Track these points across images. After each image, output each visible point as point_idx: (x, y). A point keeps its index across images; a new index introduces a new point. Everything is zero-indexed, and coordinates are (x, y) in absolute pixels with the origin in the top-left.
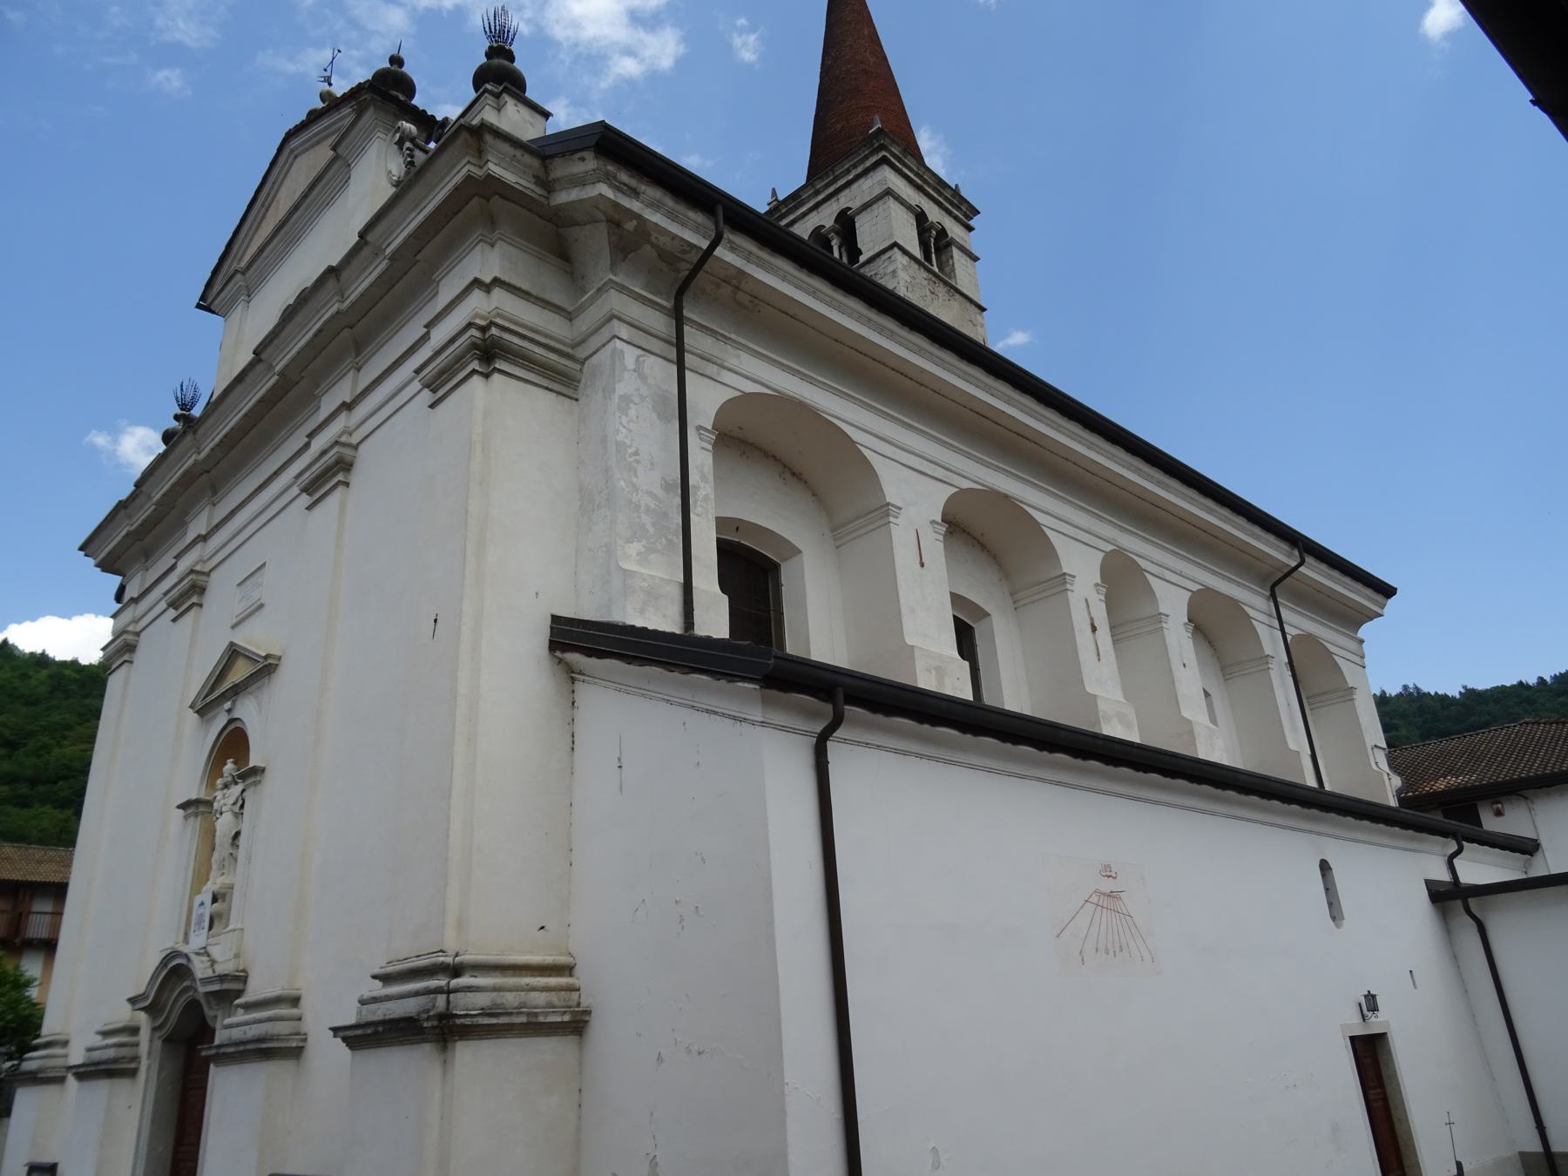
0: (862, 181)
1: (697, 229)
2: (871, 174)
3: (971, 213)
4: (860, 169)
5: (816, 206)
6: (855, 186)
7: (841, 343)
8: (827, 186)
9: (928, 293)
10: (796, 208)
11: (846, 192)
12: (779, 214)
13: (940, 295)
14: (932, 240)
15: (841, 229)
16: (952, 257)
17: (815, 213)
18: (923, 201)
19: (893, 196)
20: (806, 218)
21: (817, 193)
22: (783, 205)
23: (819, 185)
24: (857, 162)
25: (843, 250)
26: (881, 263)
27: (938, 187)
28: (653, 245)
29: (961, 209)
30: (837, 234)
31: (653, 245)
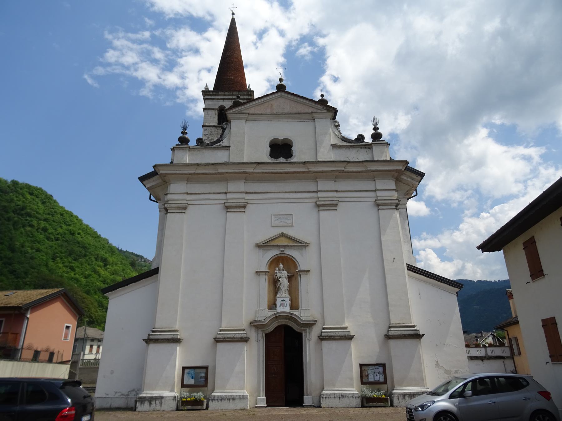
5: (224, 99)
10: (215, 95)
17: (222, 101)
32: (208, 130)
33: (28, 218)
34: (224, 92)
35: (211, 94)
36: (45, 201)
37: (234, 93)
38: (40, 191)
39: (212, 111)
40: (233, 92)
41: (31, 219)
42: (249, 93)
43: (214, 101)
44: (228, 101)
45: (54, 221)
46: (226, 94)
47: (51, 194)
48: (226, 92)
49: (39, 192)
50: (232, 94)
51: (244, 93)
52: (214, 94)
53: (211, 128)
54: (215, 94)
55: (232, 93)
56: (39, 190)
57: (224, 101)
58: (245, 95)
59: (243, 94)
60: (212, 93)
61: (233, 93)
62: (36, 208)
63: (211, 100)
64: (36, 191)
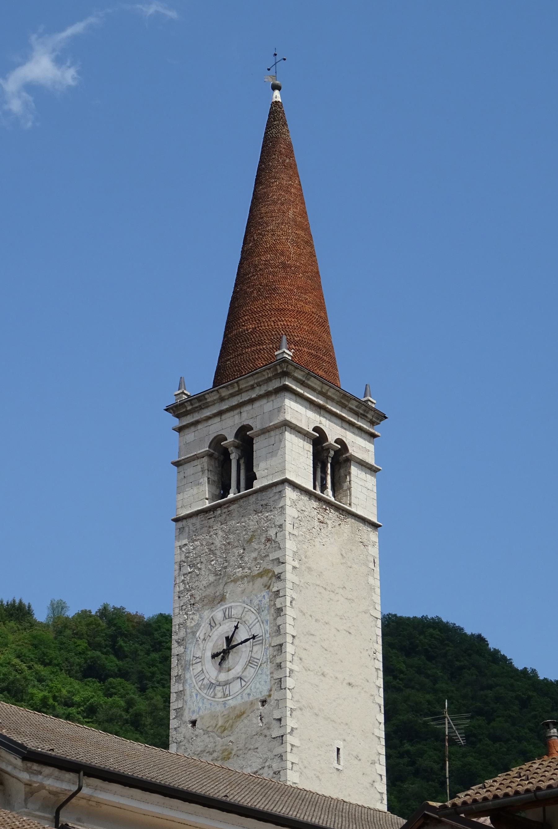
0: (264, 401)
1: (69, 781)
2: (273, 397)
3: (378, 419)
4: (262, 390)
5: (220, 413)
6: (257, 404)
7: (147, 815)
8: (232, 395)
9: (316, 523)
10: (200, 408)
11: (248, 408)
12: (184, 410)
13: (329, 522)
14: (330, 460)
15: (240, 443)
16: (350, 473)
17: (217, 419)
18: (323, 420)
19: (289, 426)
20: (210, 422)
21: (222, 399)
22: (189, 403)
23: (225, 393)
24: (261, 381)
25: (242, 462)
26: (271, 495)
27: (343, 401)
28: (46, 790)
29: (366, 417)
30: (237, 447)
31: (46, 790)
32: (187, 529)
33: (407, 746)
34: (217, 390)
35: (189, 408)
36: (458, 663)
37: (240, 382)
38: (436, 632)
39: (195, 463)
40: (237, 382)
41: (420, 746)
42: (278, 367)
43: (200, 427)
44: (231, 414)
45: (495, 739)
46: (223, 394)
47: (476, 632)
48: (221, 390)
49: (431, 636)
50: (237, 389)
51: (265, 373)
52: (197, 407)
53: (194, 520)
54: (197, 405)
55: (236, 385)
56: (431, 630)
57: (224, 417)
58: (269, 380)
59: (263, 378)
60: (192, 404)
61: (238, 386)
62: (429, 702)
63: (193, 429)
64: (422, 637)
